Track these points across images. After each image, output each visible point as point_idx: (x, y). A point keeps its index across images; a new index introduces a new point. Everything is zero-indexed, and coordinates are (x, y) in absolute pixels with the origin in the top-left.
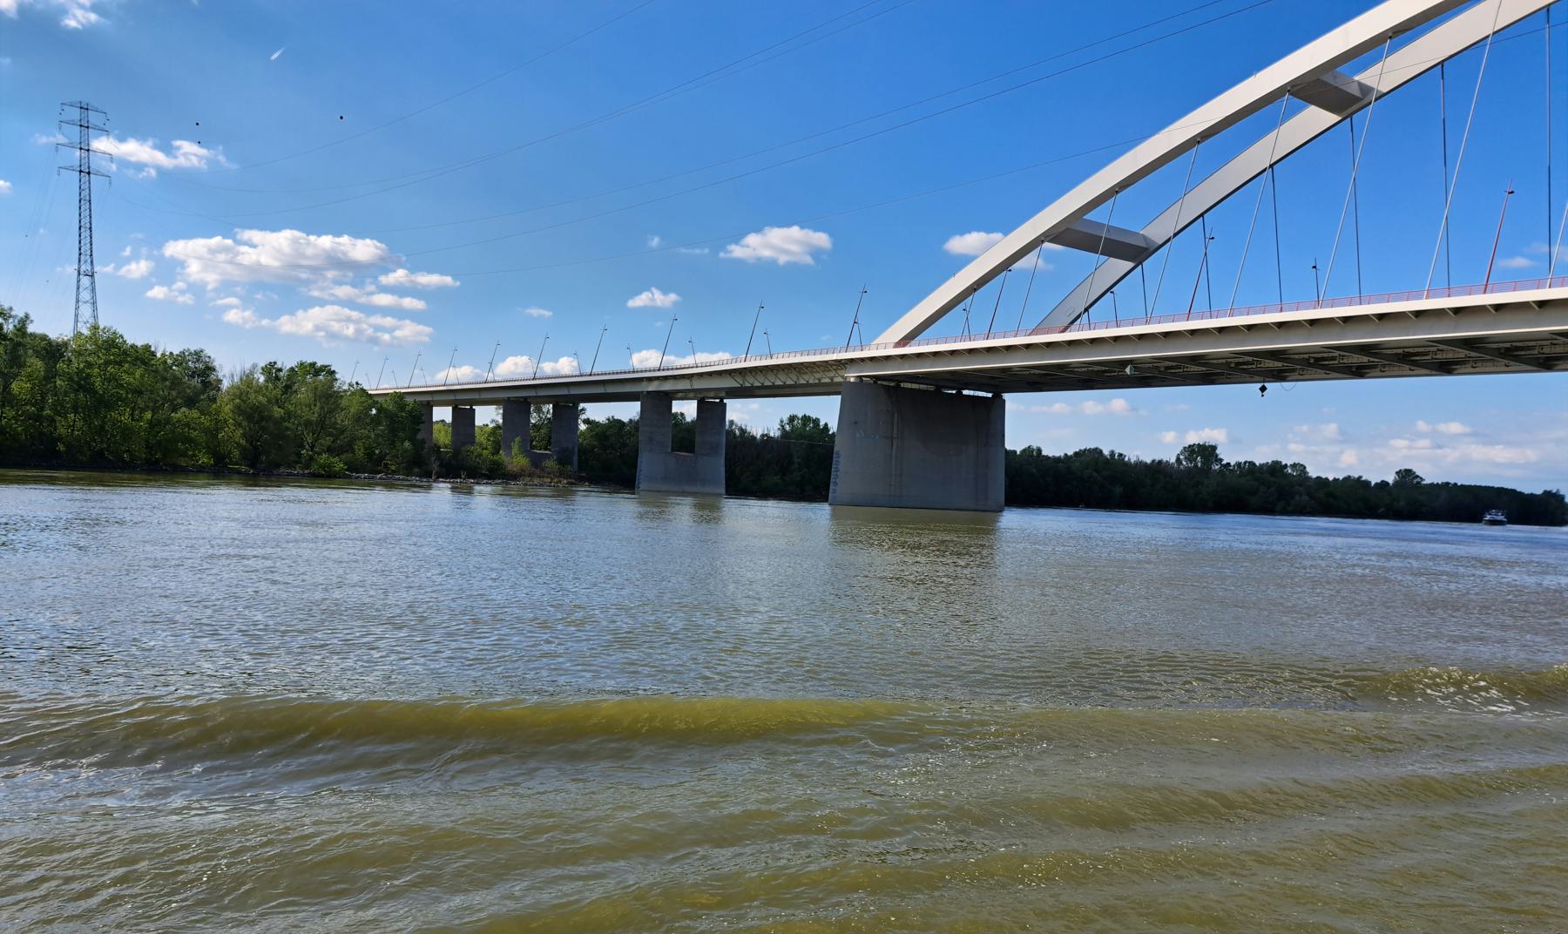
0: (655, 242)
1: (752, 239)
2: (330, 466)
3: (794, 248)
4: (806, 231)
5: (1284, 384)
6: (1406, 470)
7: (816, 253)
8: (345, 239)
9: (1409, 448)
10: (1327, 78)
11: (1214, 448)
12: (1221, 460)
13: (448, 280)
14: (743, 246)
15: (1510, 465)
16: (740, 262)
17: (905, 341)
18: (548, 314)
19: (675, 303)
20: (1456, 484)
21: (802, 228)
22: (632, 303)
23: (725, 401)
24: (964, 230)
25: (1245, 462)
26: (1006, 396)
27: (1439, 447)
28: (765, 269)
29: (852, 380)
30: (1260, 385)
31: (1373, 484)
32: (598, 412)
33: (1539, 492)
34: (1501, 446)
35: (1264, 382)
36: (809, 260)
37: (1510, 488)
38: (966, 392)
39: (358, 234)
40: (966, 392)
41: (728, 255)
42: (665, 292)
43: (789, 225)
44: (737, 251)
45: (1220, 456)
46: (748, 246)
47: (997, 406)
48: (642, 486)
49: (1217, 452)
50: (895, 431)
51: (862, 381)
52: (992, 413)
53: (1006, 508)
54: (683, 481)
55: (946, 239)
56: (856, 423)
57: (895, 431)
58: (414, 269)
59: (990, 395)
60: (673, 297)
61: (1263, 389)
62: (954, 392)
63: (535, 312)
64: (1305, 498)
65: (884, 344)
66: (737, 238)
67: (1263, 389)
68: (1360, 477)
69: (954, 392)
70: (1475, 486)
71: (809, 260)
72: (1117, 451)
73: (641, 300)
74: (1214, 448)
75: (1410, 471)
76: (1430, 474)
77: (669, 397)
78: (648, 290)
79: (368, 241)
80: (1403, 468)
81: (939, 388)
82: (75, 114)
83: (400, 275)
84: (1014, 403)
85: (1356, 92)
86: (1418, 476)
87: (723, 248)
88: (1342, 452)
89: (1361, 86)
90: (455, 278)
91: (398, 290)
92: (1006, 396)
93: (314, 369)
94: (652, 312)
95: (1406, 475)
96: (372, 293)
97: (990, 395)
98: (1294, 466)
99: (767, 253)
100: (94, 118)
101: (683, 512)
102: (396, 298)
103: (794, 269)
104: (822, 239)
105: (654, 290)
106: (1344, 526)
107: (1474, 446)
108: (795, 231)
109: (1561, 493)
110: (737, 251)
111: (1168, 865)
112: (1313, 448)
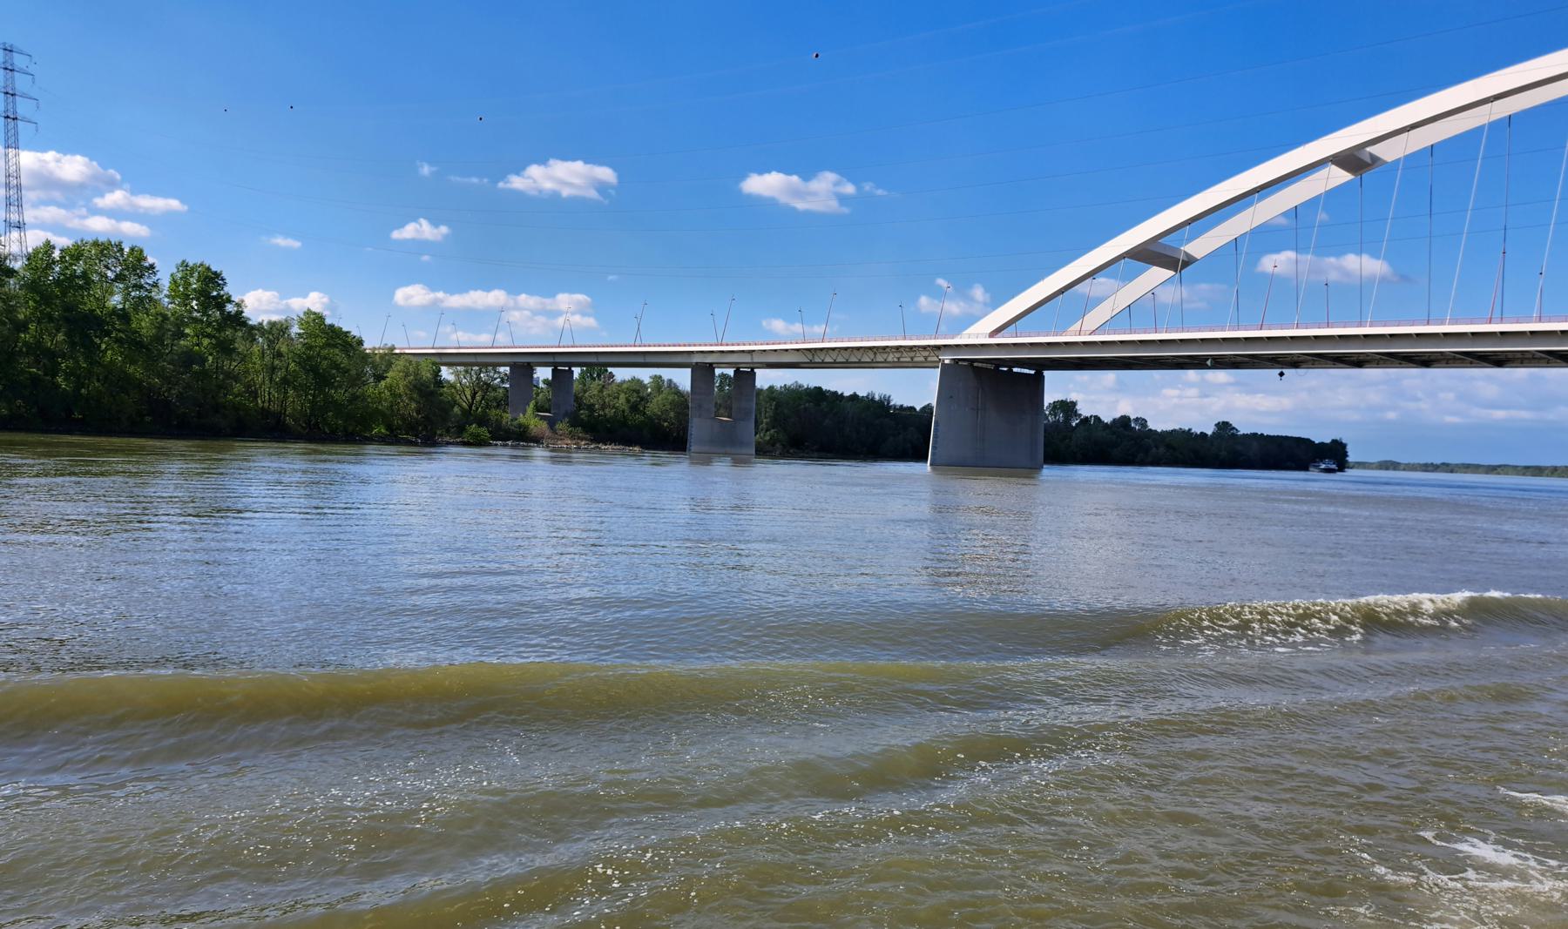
0: (426, 170)
1: (535, 171)
2: (479, 435)
3: (576, 181)
4: (589, 166)
5: (1298, 370)
6: (1223, 422)
7: (602, 187)
8: (50, 156)
9: (1180, 397)
10: (1356, 153)
11: (1074, 404)
12: (1080, 415)
13: (174, 204)
14: (523, 177)
15: (1268, 413)
16: (519, 195)
18: (297, 244)
19: (446, 237)
20: (1262, 434)
21: (586, 162)
22: (396, 235)
23: (755, 370)
24: (762, 170)
25: (1091, 416)
26: (1046, 373)
27: (1207, 396)
28: (551, 205)
29: (947, 362)
31: (918, 409)
32: (621, 374)
33: (1328, 441)
34: (1260, 395)
35: (1282, 368)
36: (593, 194)
37: (1284, 435)
38: (1015, 370)
39: (67, 148)
40: (1015, 370)
41: (508, 186)
42: (435, 223)
43: (574, 159)
44: (517, 182)
45: (1079, 412)
46: (529, 177)
47: (1038, 380)
48: (693, 448)
49: (1078, 407)
50: (980, 405)
51: (972, 365)
52: (1036, 385)
53: (1045, 466)
54: (727, 445)
55: (743, 176)
56: (951, 397)
57: (980, 405)
58: (135, 191)
59: (1032, 372)
60: (444, 229)
61: (1281, 374)
62: (1005, 369)
63: (281, 241)
64: (1162, 450)
65: (978, 333)
66: (519, 170)
67: (1281, 374)
68: (1190, 430)
69: (1005, 369)
70: (1278, 436)
71: (593, 194)
73: (409, 231)
74: (1074, 404)
75: (1227, 423)
76: (1244, 426)
78: (415, 219)
79: (78, 158)
80: (1221, 421)
83: (116, 197)
85: (1368, 160)
86: (1234, 428)
87: (503, 176)
88: (1117, 401)
89: (1372, 156)
90: (182, 201)
92: (1046, 373)
93: (1143, 419)
94: (419, 245)
95: (1224, 427)
96: (83, 217)
97: (1032, 372)
98: (1137, 419)
99: (548, 185)
100: (19, 61)
102: (113, 222)
103: (577, 204)
104: (606, 174)
105: (422, 221)
106: (1222, 481)
107: (1237, 395)
108: (578, 166)
109: (1344, 442)
110: (517, 182)
112: (1093, 397)
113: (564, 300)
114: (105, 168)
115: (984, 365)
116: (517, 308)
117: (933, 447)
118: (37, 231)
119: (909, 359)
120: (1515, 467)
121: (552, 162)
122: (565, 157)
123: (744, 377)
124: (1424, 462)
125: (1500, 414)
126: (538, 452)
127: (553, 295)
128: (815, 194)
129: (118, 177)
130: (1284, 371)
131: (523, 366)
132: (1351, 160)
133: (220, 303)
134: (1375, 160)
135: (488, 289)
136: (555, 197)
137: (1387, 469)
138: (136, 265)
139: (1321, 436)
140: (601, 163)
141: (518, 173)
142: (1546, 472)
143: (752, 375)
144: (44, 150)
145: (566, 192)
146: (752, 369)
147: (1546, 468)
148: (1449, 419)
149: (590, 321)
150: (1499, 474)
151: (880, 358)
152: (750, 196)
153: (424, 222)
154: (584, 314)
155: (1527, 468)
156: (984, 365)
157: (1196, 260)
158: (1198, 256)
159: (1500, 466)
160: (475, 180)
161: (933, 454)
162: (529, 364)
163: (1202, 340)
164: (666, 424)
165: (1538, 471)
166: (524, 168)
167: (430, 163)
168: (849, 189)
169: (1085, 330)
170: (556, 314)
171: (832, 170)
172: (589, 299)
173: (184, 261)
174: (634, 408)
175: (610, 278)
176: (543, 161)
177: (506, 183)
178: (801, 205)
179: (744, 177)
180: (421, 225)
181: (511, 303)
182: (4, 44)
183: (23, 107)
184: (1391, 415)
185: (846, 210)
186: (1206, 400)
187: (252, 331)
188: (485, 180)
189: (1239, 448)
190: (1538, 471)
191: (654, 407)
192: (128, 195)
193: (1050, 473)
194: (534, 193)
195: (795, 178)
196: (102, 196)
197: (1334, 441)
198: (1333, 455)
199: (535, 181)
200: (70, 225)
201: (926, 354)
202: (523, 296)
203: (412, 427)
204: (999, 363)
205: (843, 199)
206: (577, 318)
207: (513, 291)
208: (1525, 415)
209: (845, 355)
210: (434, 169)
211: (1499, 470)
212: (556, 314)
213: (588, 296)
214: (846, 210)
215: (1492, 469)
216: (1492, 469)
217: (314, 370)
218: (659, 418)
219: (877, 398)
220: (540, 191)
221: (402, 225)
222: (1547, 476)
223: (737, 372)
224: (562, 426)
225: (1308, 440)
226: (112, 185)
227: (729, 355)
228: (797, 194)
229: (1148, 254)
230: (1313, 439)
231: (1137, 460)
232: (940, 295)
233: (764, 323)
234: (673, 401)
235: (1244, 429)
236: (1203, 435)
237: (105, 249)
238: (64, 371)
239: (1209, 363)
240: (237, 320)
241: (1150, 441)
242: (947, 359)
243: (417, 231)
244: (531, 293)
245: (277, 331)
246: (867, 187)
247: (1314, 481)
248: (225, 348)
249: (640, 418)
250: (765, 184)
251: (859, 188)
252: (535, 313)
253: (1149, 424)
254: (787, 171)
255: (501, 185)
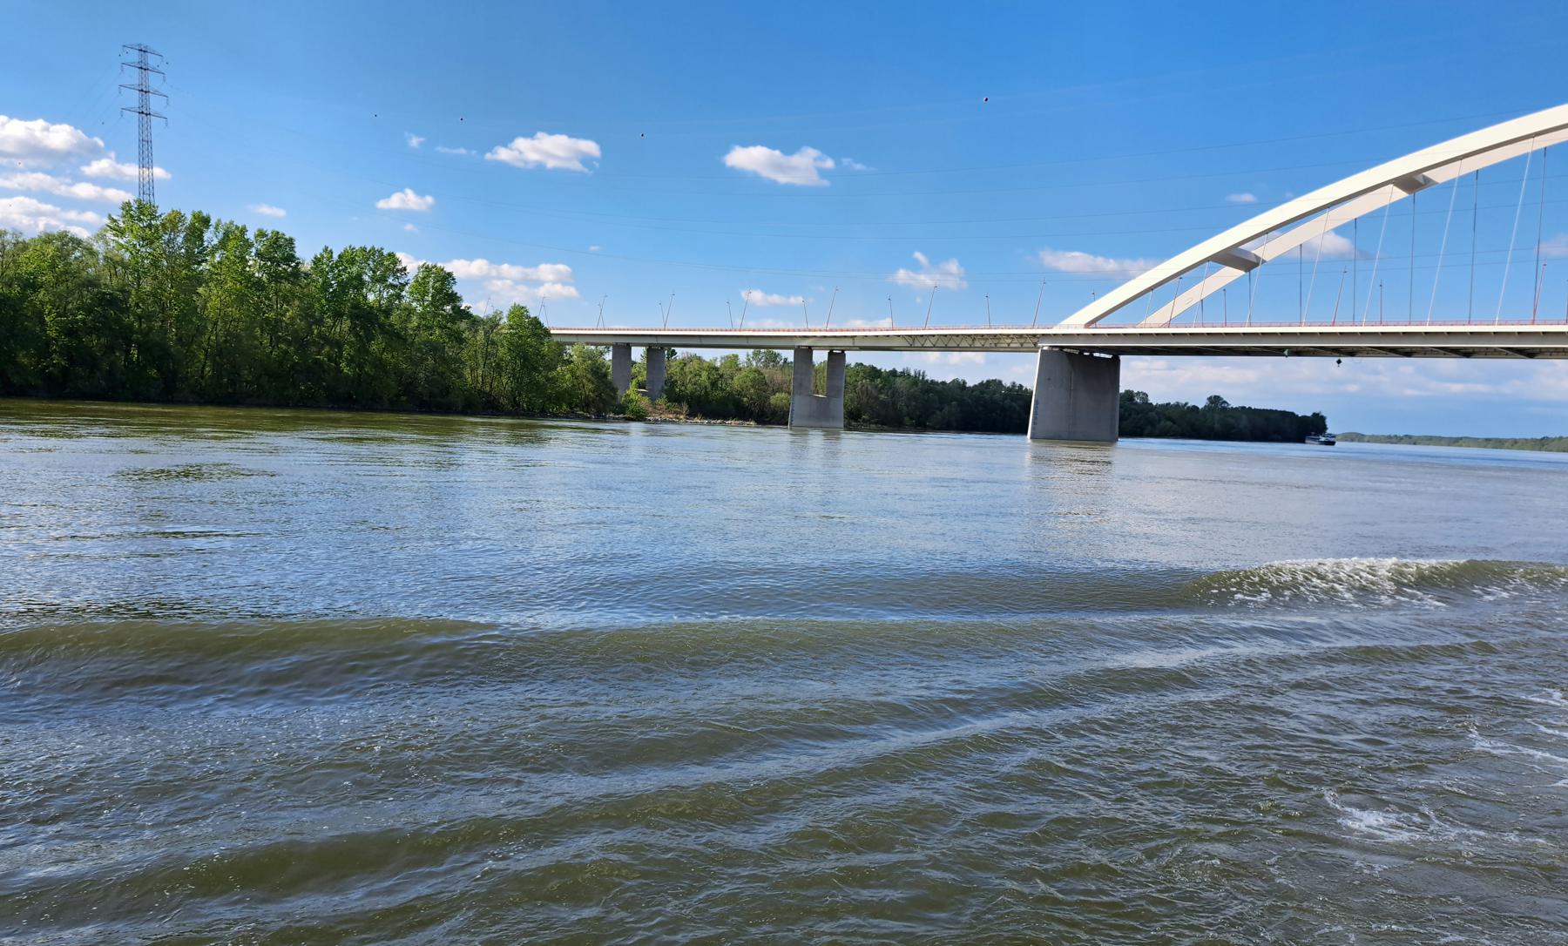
0: (415, 142)
1: (521, 143)
3: (561, 153)
5: (1355, 359)
7: (586, 160)
14: (511, 149)
16: (503, 166)
17: (1088, 325)
21: (571, 136)
22: (382, 204)
26: (1122, 358)
27: (1174, 369)
28: (538, 175)
29: (1045, 348)
30: (1337, 359)
33: (1309, 414)
37: (1269, 408)
39: (54, 118)
42: (420, 192)
44: (503, 154)
47: (1115, 363)
54: (820, 418)
59: (1110, 357)
61: (1339, 362)
66: (506, 142)
67: (1339, 362)
71: (576, 166)
72: (1018, 383)
73: (395, 201)
77: (810, 349)
78: (401, 189)
81: (1081, 353)
82: (134, 56)
83: (101, 166)
84: (1124, 359)
85: (1422, 181)
86: (1225, 402)
87: (490, 149)
91: (102, 181)
92: (1122, 358)
95: (1215, 400)
97: (1110, 357)
99: (533, 156)
100: (152, 60)
101: (816, 440)
102: (98, 189)
104: (590, 147)
110: (503, 154)
111: (253, 935)
113: (546, 271)
114: (90, 135)
115: (1072, 351)
116: (500, 277)
117: (1034, 423)
118: (22, 198)
119: (1018, 345)
120: (1476, 440)
121: (539, 134)
122: (552, 131)
123: (836, 357)
124: (1387, 434)
125: (1457, 388)
126: (636, 427)
127: (535, 264)
128: (794, 168)
129: (101, 143)
130: (1342, 359)
131: (622, 348)
132: (1410, 183)
133: (453, 298)
134: (1428, 181)
135: (470, 258)
136: (540, 167)
137: (1352, 440)
138: (387, 266)
139: (1303, 410)
140: (586, 137)
141: (505, 146)
142: (1507, 444)
143: (843, 354)
144: (32, 118)
145: (551, 164)
146: (843, 351)
147: (1507, 441)
148: (1408, 392)
149: (571, 291)
150: (1461, 446)
151: (977, 344)
152: (732, 169)
153: (409, 192)
154: (564, 284)
155: (1488, 440)
156: (1072, 351)
157: (1264, 261)
158: (1267, 260)
159: (1461, 438)
160: (462, 151)
161: (1033, 429)
162: (628, 344)
163: (1263, 334)
164: (745, 399)
165: (1499, 443)
166: (512, 140)
167: (418, 135)
168: (829, 164)
169: (1156, 322)
170: (538, 283)
171: (815, 147)
172: (569, 269)
173: (326, 248)
174: (714, 384)
175: (593, 248)
176: (530, 134)
177: (493, 154)
178: (782, 179)
179: (727, 151)
180: (406, 195)
181: (494, 273)
182: (140, 45)
183: (155, 103)
184: (1353, 388)
185: (826, 183)
186: (1174, 372)
187: (475, 322)
188: (474, 152)
189: (1231, 421)
190: (1499, 443)
191: (736, 383)
192: (113, 163)
193: (1124, 443)
194: (520, 164)
195: (777, 152)
196: (88, 164)
197: (1316, 415)
198: (1306, 429)
199: (521, 153)
200: (57, 192)
201: (1009, 341)
202: (505, 266)
203: (586, 404)
204: (1082, 349)
205: (823, 173)
206: (558, 287)
207: (496, 260)
208: (1481, 388)
209: (958, 340)
210: (422, 139)
211: (1461, 442)
212: (538, 283)
213: (568, 265)
214: (826, 183)
215: (1455, 441)
216: (1455, 441)
217: (525, 358)
218: (739, 393)
219: (912, 374)
220: (526, 162)
221: (388, 195)
222: (1508, 448)
223: (831, 354)
224: (662, 402)
225: (1293, 413)
226: (96, 153)
227: (843, 339)
228: (780, 168)
229: (1230, 257)
230: (1296, 413)
231: (1146, 432)
232: (915, 267)
233: (743, 294)
234: (754, 378)
235: (1234, 403)
236: (1195, 408)
237: (369, 254)
238: (346, 359)
239: (1286, 352)
240: (465, 315)
241: (1153, 413)
242: (1045, 346)
243: (403, 201)
244: (513, 263)
245: (493, 323)
246: (846, 161)
247: (1310, 449)
248: (458, 338)
249: (719, 394)
250: (748, 158)
251: (838, 163)
252: (517, 282)
253: (1149, 398)
254: (772, 146)
255: (488, 156)
